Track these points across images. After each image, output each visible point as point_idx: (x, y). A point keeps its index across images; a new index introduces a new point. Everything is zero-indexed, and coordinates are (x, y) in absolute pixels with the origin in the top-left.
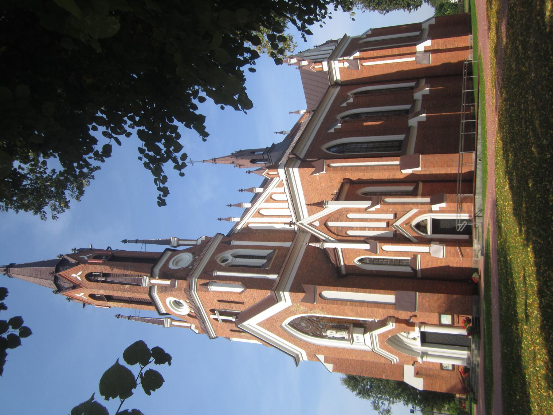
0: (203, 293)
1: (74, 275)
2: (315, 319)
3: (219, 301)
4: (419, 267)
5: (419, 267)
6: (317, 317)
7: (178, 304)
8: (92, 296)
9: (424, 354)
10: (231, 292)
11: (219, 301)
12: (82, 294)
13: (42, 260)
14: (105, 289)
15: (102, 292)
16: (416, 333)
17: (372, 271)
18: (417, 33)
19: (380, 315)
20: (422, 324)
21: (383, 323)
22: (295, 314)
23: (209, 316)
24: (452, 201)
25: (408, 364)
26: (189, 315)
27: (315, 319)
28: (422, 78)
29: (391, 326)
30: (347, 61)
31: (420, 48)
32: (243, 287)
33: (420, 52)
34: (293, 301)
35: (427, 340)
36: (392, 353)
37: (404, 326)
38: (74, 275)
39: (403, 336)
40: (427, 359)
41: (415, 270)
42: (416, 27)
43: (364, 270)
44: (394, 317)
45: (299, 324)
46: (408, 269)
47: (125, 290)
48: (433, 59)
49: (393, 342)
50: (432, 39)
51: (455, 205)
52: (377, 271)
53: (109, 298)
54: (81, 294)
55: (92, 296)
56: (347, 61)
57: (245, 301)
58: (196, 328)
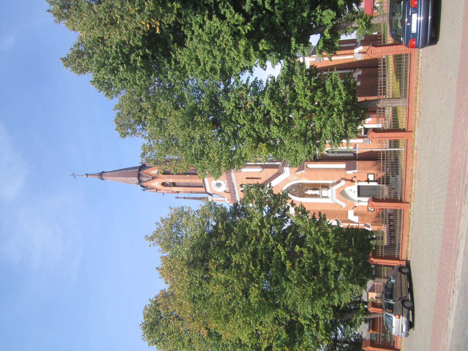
0: (238, 173)
1: (152, 172)
2: (301, 185)
3: (247, 178)
4: (357, 152)
5: (357, 152)
6: (302, 184)
7: (219, 185)
8: (164, 184)
9: (359, 201)
10: (253, 172)
11: (247, 178)
12: (157, 183)
13: (122, 168)
14: (173, 178)
15: (171, 181)
16: (354, 188)
17: (332, 157)
18: (354, 44)
19: (338, 176)
20: (359, 181)
21: (338, 182)
22: (291, 182)
23: (238, 189)
24: (374, 117)
25: (350, 210)
26: (225, 191)
27: (301, 185)
28: (357, 68)
29: (343, 183)
30: (314, 57)
31: (356, 50)
32: (261, 168)
33: (356, 53)
34: (291, 173)
35: (361, 194)
36: (342, 201)
37: (350, 182)
38: (152, 172)
39: (347, 190)
40: (360, 204)
41: (355, 154)
42: (353, 41)
43: (329, 156)
44: (344, 178)
45: (291, 190)
46: (352, 155)
47: (186, 178)
48: (364, 57)
49: (343, 194)
50: (363, 46)
51: (375, 119)
52: (335, 157)
53: (174, 185)
54: (156, 184)
55: (164, 184)
56: (314, 57)
57: (262, 177)
58: (228, 200)
